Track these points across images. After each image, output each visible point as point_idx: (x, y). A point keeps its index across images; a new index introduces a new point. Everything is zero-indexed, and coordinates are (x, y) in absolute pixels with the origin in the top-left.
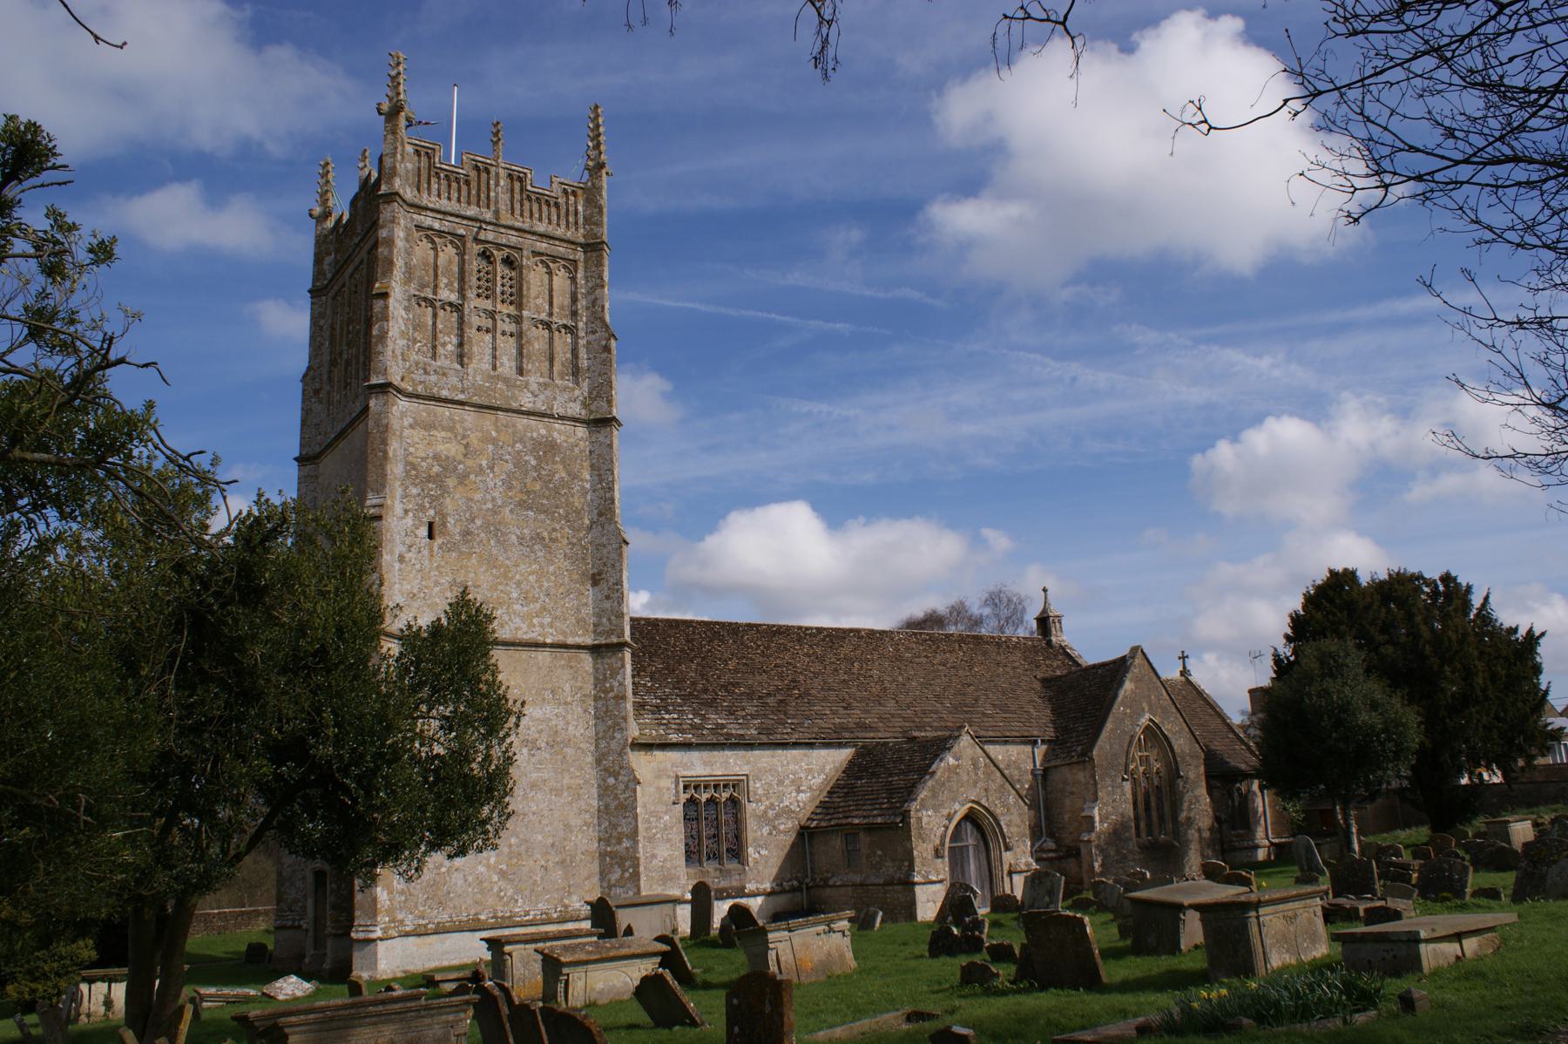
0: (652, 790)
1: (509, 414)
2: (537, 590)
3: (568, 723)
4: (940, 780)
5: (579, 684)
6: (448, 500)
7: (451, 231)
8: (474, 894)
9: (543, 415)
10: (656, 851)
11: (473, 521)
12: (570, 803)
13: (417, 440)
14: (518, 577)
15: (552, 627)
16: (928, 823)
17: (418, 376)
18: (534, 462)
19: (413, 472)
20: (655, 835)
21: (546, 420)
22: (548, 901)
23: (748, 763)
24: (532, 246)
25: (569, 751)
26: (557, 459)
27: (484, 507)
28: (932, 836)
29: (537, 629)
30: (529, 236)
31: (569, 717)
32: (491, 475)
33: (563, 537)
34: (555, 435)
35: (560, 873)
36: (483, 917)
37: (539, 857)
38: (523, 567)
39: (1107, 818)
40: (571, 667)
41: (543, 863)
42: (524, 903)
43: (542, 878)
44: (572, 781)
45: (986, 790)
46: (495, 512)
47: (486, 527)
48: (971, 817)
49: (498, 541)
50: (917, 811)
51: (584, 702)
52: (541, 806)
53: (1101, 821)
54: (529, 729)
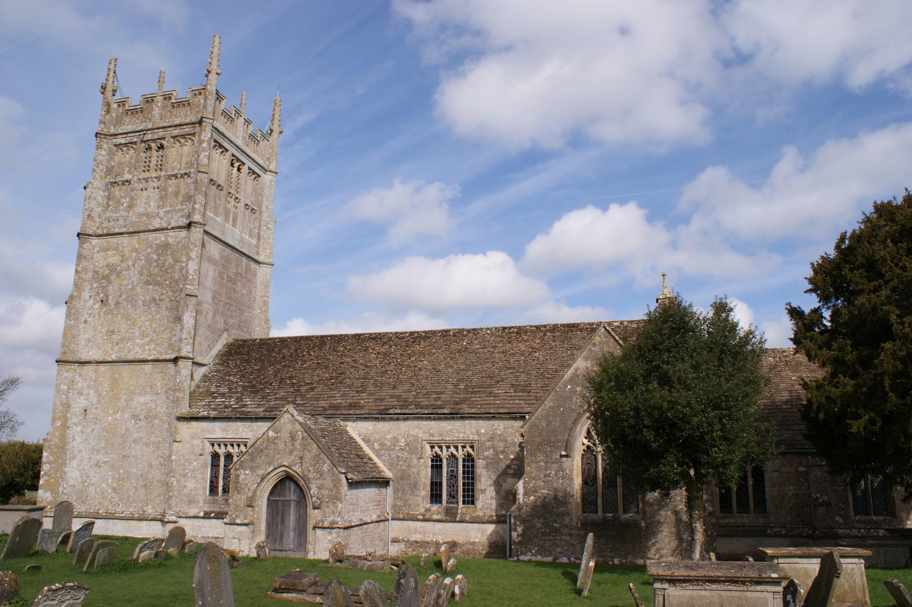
0: (189, 445)
1: (146, 233)
2: (150, 330)
3: (157, 405)
4: (259, 447)
5: (166, 382)
6: (111, 287)
7: (130, 141)
8: (99, 498)
9: (163, 229)
10: (187, 484)
11: (121, 296)
12: (153, 452)
13: (100, 258)
14: (140, 324)
15: (154, 350)
16: (245, 480)
17: (106, 224)
18: (156, 257)
19: (96, 276)
20: (187, 473)
21: (165, 231)
22: (135, 507)
23: (252, 430)
24: (171, 134)
25: (156, 421)
26: (169, 253)
27: (128, 287)
28: (247, 490)
29: (147, 352)
30: (169, 129)
31: (158, 401)
32: (133, 270)
33: (166, 297)
34: (169, 239)
35: (143, 491)
36: (101, 512)
37: (133, 481)
38: (143, 317)
39: (535, 492)
40: (163, 373)
41: (135, 485)
42: (123, 506)
43: (133, 493)
44: (156, 439)
45: (301, 458)
46: (132, 289)
47: (127, 299)
48: (287, 478)
49: (132, 305)
50: (236, 470)
51: (167, 392)
52: (138, 453)
53: (525, 494)
54: (136, 409)
